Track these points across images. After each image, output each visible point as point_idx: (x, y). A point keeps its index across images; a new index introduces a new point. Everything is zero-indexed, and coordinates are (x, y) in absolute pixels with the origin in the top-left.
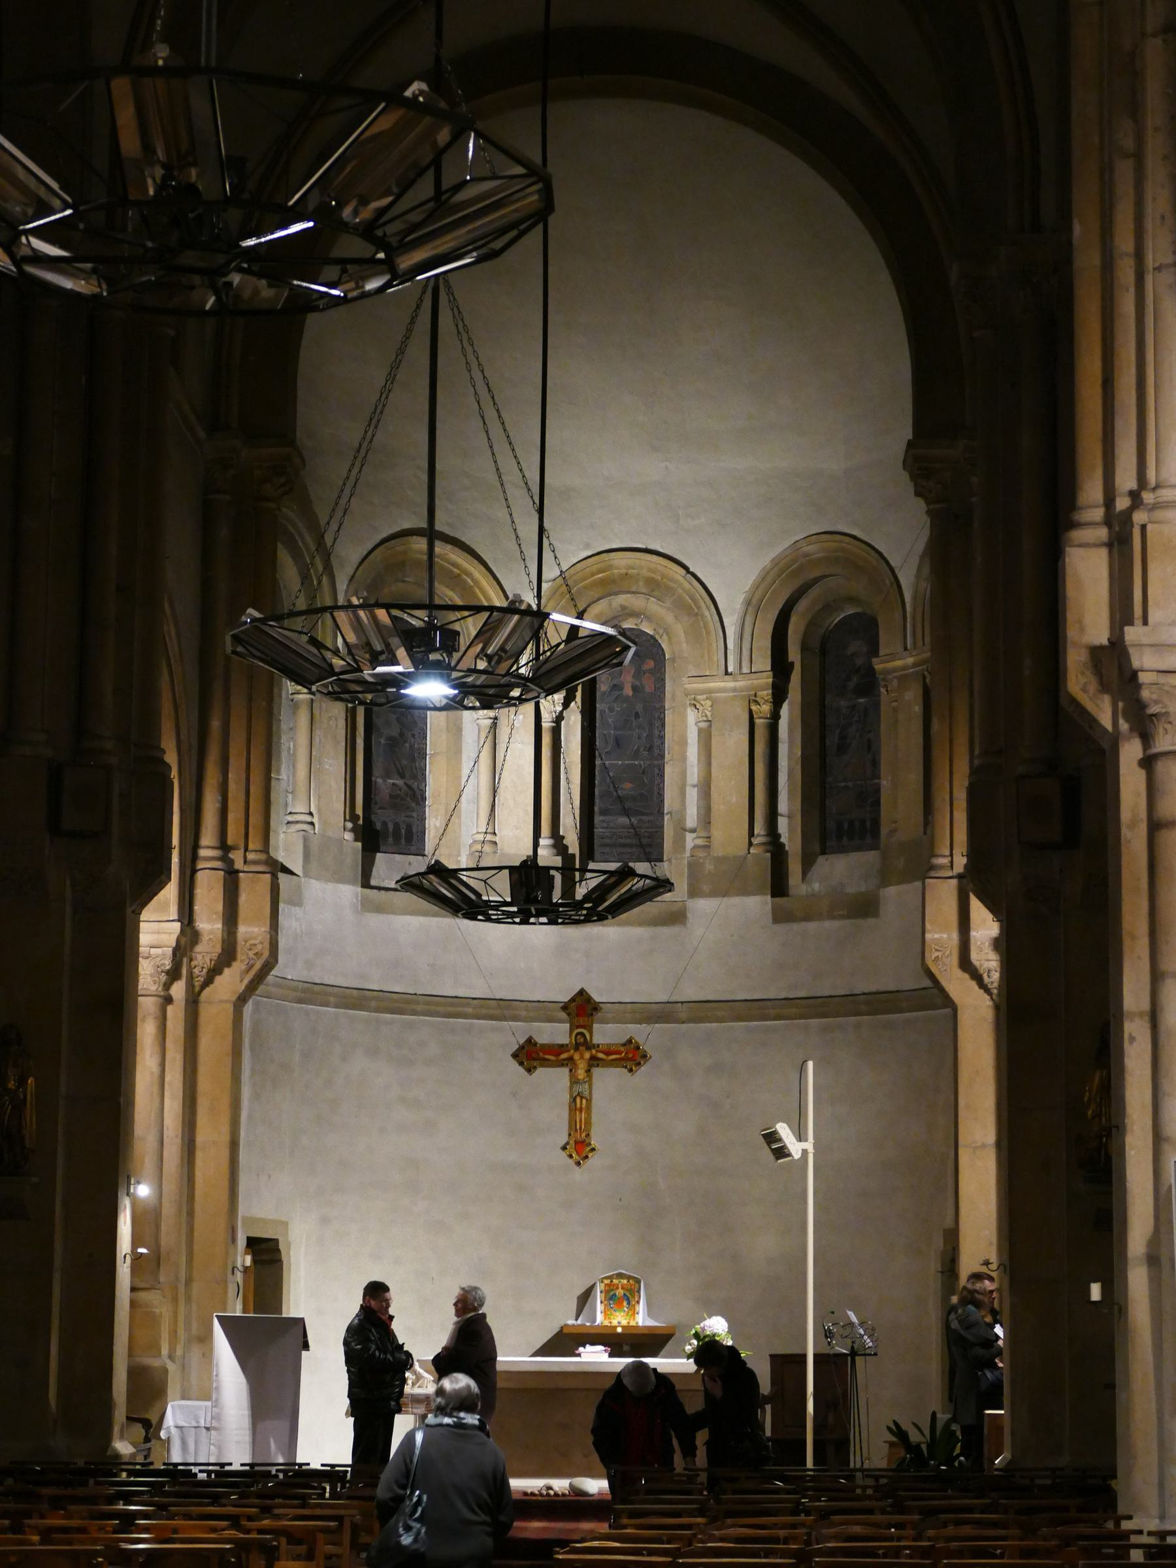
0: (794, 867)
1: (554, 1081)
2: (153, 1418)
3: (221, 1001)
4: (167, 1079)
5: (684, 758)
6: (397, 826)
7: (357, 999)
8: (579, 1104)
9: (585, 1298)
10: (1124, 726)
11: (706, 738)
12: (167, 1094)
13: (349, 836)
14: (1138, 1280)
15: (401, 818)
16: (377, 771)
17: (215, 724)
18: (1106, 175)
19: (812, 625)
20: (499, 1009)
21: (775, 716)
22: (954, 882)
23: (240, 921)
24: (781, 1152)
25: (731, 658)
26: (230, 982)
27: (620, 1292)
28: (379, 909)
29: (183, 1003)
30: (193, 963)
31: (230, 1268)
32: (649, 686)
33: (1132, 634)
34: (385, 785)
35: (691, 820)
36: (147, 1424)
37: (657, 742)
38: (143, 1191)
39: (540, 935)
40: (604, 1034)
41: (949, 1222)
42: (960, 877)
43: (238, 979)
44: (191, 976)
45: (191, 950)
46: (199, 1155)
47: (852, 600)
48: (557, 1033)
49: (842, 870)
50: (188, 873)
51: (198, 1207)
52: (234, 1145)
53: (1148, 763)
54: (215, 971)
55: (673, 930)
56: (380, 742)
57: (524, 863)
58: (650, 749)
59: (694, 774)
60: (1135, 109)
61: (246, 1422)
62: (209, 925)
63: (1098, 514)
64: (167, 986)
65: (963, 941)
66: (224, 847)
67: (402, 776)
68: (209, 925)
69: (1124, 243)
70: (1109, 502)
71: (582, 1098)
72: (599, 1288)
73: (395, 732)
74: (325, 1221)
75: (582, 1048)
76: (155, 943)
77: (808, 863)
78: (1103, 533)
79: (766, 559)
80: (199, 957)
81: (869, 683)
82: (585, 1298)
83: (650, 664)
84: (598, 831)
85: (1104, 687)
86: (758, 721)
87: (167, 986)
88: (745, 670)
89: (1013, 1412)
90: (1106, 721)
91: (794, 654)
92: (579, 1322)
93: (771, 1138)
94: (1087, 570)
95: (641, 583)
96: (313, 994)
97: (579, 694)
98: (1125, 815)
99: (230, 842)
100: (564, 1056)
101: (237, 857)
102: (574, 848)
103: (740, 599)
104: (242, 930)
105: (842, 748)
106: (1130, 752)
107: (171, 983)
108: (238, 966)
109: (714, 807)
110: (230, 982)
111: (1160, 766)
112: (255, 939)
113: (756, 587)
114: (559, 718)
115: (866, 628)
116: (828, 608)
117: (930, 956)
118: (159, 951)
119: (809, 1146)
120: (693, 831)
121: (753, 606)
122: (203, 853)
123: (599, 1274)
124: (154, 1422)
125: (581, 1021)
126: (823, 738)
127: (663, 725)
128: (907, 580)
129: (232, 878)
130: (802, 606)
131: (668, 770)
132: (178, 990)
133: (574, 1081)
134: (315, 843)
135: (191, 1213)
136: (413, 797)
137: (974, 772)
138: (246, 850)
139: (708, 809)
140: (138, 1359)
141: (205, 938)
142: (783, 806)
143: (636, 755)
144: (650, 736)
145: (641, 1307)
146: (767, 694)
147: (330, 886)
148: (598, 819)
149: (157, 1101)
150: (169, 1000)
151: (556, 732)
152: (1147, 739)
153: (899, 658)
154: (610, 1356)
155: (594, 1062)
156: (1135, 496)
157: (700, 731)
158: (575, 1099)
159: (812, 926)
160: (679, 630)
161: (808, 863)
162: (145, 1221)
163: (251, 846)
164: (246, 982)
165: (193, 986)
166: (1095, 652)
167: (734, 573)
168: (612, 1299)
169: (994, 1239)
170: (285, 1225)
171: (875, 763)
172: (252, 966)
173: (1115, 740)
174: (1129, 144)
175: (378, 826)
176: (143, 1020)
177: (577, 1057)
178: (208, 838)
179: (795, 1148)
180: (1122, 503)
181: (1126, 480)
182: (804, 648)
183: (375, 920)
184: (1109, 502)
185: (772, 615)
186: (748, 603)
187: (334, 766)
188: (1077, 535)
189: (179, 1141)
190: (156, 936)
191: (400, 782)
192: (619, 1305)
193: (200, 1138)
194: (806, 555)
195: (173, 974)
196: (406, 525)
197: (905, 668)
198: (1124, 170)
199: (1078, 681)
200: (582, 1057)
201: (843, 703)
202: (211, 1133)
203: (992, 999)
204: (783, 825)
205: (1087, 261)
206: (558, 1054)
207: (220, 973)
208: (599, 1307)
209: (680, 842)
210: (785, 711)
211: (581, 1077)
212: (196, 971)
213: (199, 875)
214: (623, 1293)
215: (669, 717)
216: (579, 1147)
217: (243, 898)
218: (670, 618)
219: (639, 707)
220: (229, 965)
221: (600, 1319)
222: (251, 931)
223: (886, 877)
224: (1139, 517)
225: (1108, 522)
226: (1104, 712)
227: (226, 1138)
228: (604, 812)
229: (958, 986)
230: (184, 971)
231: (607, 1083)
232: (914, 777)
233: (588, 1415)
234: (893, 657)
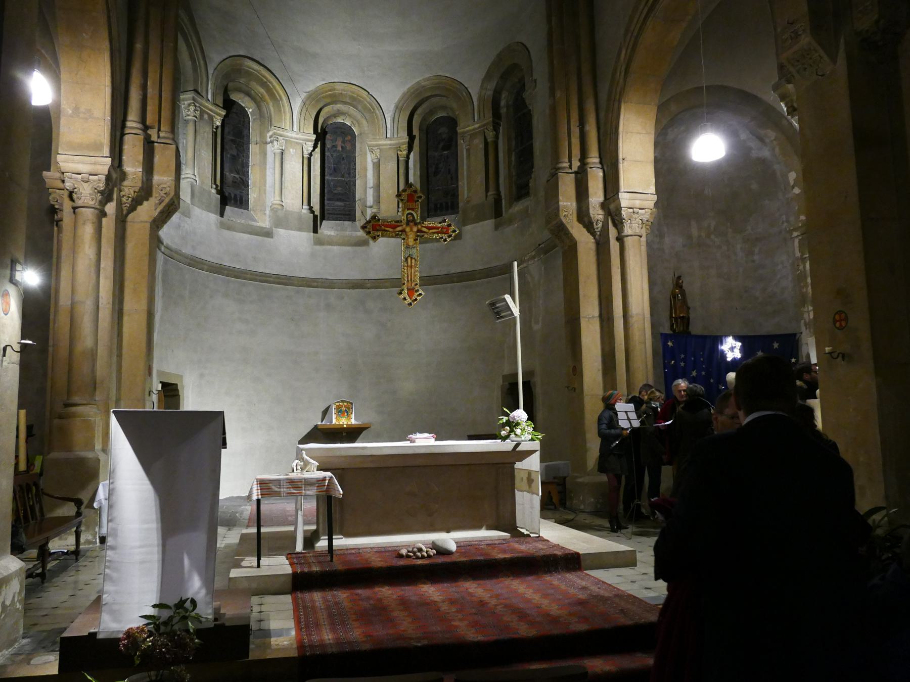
2: (84, 496)
4: (102, 266)
5: (366, 176)
6: (235, 195)
7: (217, 269)
9: (326, 412)
11: (377, 166)
12: (101, 275)
13: (214, 191)
15: (238, 192)
16: (227, 166)
17: (139, 46)
19: (424, 119)
21: (408, 157)
22: (573, 175)
23: (155, 172)
25: (389, 131)
26: (147, 211)
27: (343, 409)
29: (114, 217)
30: (122, 193)
31: (147, 393)
32: (348, 147)
34: (230, 176)
35: (370, 200)
36: (79, 503)
37: (352, 171)
42: (576, 173)
44: (120, 204)
45: (120, 185)
46: (126, 319)
47: (444, 108)
50: (118, 134)
51: (124, 351)
52: (150, 315)
54: (137, 202)
55: (363, 248)
56: (227, 156)
58: (349, 174)
59: (371, 181)
61: (154, 555)
62: (133, 168)
64: (103, 203)
66: (143, 120)
67: (238, 174)
68: (133, 168)
71: (412, 258)
72: (334, 407)
73: (234, 152)
74: (202, 376)
75: (411, 224)
79: (405, 89)
80: (126, 189)
82: (326, 412)
83: (349, 138)
84: (326, 207)
86: (401, 159)
87: (103, 203)
88: (395, 136)
91: (416, 132)
97: (319, 145)
99: (148, 123)
100: (399, 229)
101: (153, 133)
102: (317, 212)
103: (392, 107)
104: (156, 178)
105: (436, 173)
107: (106, 204)
108: (153, 201)
109: (381, 194)
110: (147, 211)
113: (399, 101)
114: (311, 155)
116: (431, 112)
118: (96, 177)
120: (371, 207)
121: (399, 108)
122: (129, 124)
124: (86, 502)
125: (411, 205)
126: (428, 169)
129: (149, 147)
130: (419, 111)
131: (358, 182)
132: (110, 208)
134: (197, 190)
135: (120, 356)
136: (243, 183)
138: (159, 130)
139: (379, 196)
140: (77, 453)
141: (130, 177)
143: (343, 176)
144: (349, 169)
146: (405, 147)
147: (204, 212)
148: (326, 202)
149: (94, 276)
150: (104, 214)
151: (309, 160)
154: (436, 440)
157: (374, 163)
158: (406, 259)
163: (162, 129)
164: (159, 210)
165: (122, 210)
167: (389, 96)
168: (340, 412)
169: (600, 367)
170: (182, 377)
175: (227, 194)
176: (84, 224)
177: (408, 229)
178: (133, 123)
182: (420, 129)
185: (408, 113)
186: (397, 107)
187: (206, 155)
189: (110, 306)
190: (93, 166)
191: (237, 176)
192: (343, 415)
193: (127, 307)
194: (424, 87)
195: (106, 196)
196: (242, 53)
197: (474, 129)
200: (411, 230)
201: (436, 154)
202: (134, 305)
203: (595, 238)
206: (394, 227)
207: (141, 204)
208: (334, 416)
210: (412, 155)
211: (411, 244)
212: (124, 199)
213: (126, 138)
215: (358, 160)
217: (157, 159)
219: (344, 155)
220: (147, 200)
222: (162, 179)
227: (144, 306)
228: (329, 200)
230: (115, 196)
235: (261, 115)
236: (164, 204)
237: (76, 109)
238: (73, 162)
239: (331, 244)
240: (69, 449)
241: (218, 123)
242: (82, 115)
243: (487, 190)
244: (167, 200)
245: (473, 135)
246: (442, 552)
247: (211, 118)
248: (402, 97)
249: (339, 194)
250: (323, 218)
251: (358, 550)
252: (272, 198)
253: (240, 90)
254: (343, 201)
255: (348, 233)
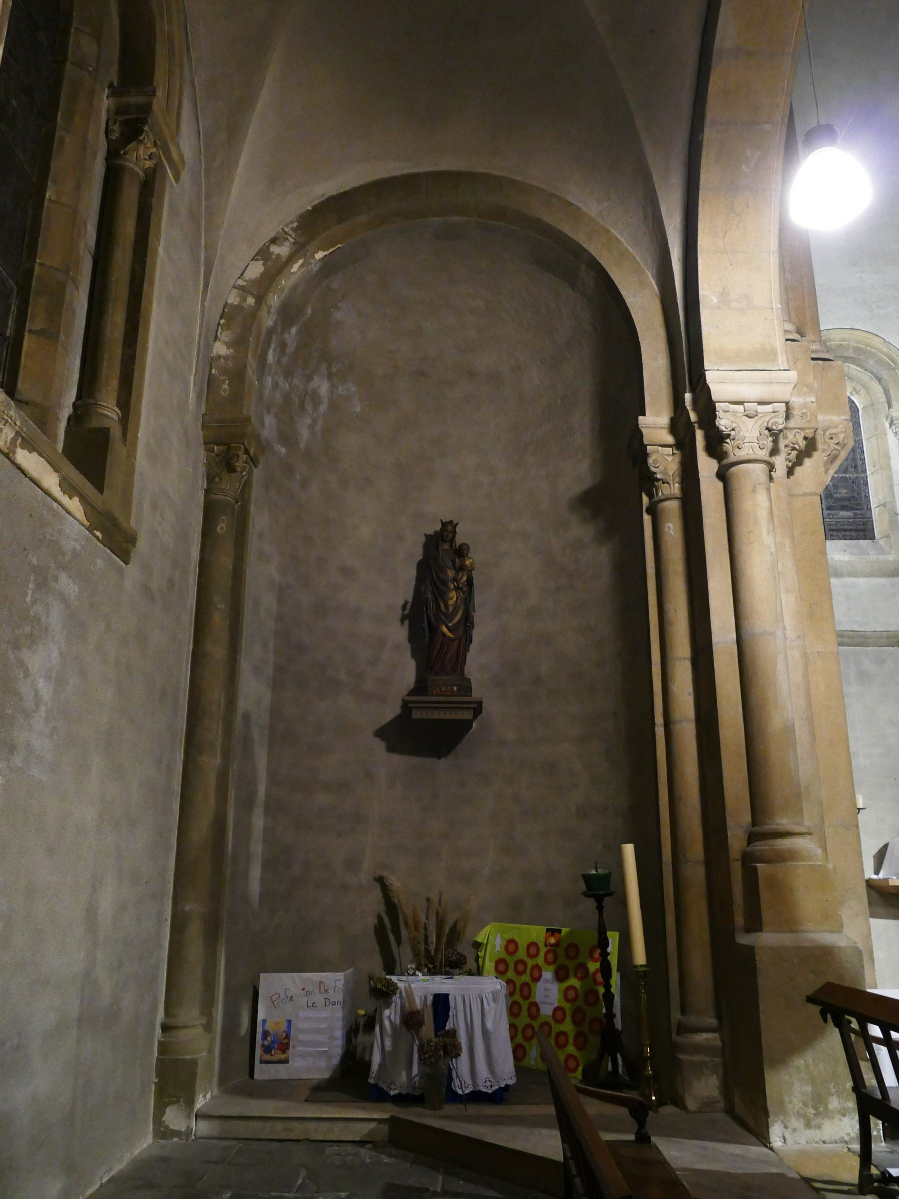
3: (805, 494)
37: (859, 463)
43: (822, 469)
57: (383, 739)
58: (856, 467)
76: (766, 398)
92: (881, 875)
95: (851, 351)
108: (819, 457)
112: (837, 427)
118: (769, 408)
127: (863, 452)
164: (831, 472)
172: (836, 457)
176: (754, 491)
236: (838, 462)
237: (724, 294)
238: (733, 381)
239: (853, 574)
240: (790, 924)
242: (734, 305)
244: (843, 455)
249: (844, 499)
251: (219, 975)
254: (852, 509)
255: (872, 557)
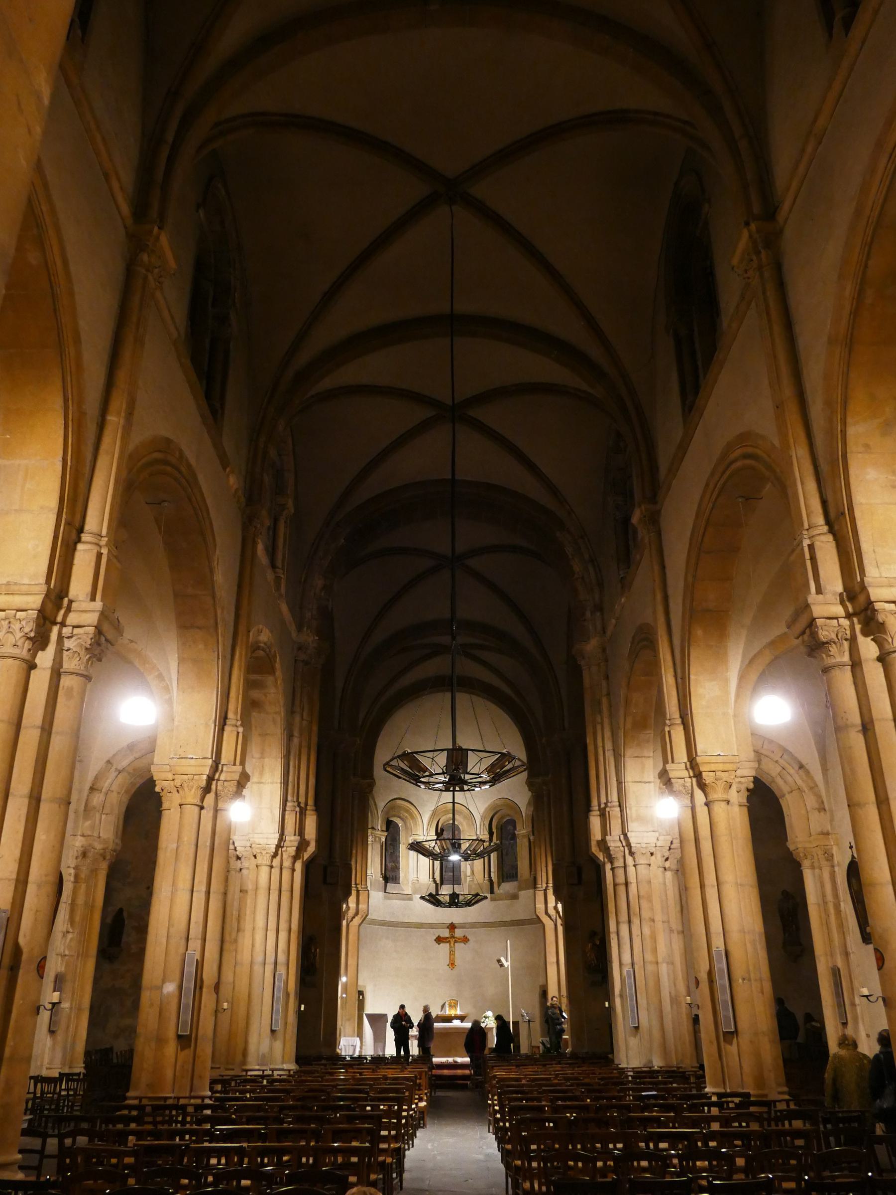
0: (496, 886)
1: (445, 947)
8: (452, 953)
9: (443, 1006)
10: (606, 860)
14: (618, 1001)
18: (595, 728)
20: (432, 926)
24: (502, 965)
26: (357, 920)
28: (389, 899)
33: (608, 838)
34: (390, 865)
35: (469, 873)
38: (344, 979)
39: (453, 910)
40: (458, 933)
41: (541, 982)
47: (508, 815)
48: (446, 933)
49: (508, 887)
53: (613, 869)
54: (354, 917)
60: (600, 712)
63: (597, 808)
65: (549, 906)
66: (356, 884)
69: (600, 744)
70: (599, 805)
77: (499, 885)
78: (598, 813)
79: (486, 805)
81: (514, 837)
82: (443, 1006)
85: (600, 851)
89: (572, 1037)
90: (601, 858)
91: (494, 830)
93: (499, 961)
94: (595, 822)
96: (374, 922)
98: (608, 882)
101: (359, 886)
102: (438, 881)
106: (608, 867)
108: (359, 916)
111: (616, 870)
115: (513, 823)
116: (502, 817)
117: (538, 911)
119: (509, 963)
123: (447, 999)
128: (523, 810)
133: (450, 947)
136: (396, 868)
137: (553, 865)
142: (492, 870)
145: (458, 1008)
152: (612, 863)
153: (522, 831)
155: (456, 942)
156: (606, 804)
159: (501, 902)
160: (465, 823)
161: (499, 885)
162: (345, 990)
166: (598, 842)
168: (450, 1006)
171: (516, 858)
173: (604, 864)
174: (599, 720)
178: (297, 702)
179: (506, 964)
180: (603, 806)
181: (603, 800)
183: (389, 902)
184: (599, 805)
188: (592, 813)
198: (599, 727)
199: (594, 849)
204: (492, 875)
205: (591, 748)
209: (466, 879)
214: (453, 1006)
216: (452, 964)
218: (462, 820)
221: (447, 1013)
222: (362, 906)
223: (520, 888)
224: (607, 809)
225: (600, 810)
226: (601, 856)
229: (545, 919)
231: (459, 946)
232: (527, 862)
233: (462, 1040)
234: (520, 830)
235: (406, 828)
241: (383, 840)
243: (811, 547)
245: (523, 836)
246: (455, 1062)
247: (380, 839)
248: (486, 809)
250: (442, 883)
252: (412, 876)
253: (394, 816)
